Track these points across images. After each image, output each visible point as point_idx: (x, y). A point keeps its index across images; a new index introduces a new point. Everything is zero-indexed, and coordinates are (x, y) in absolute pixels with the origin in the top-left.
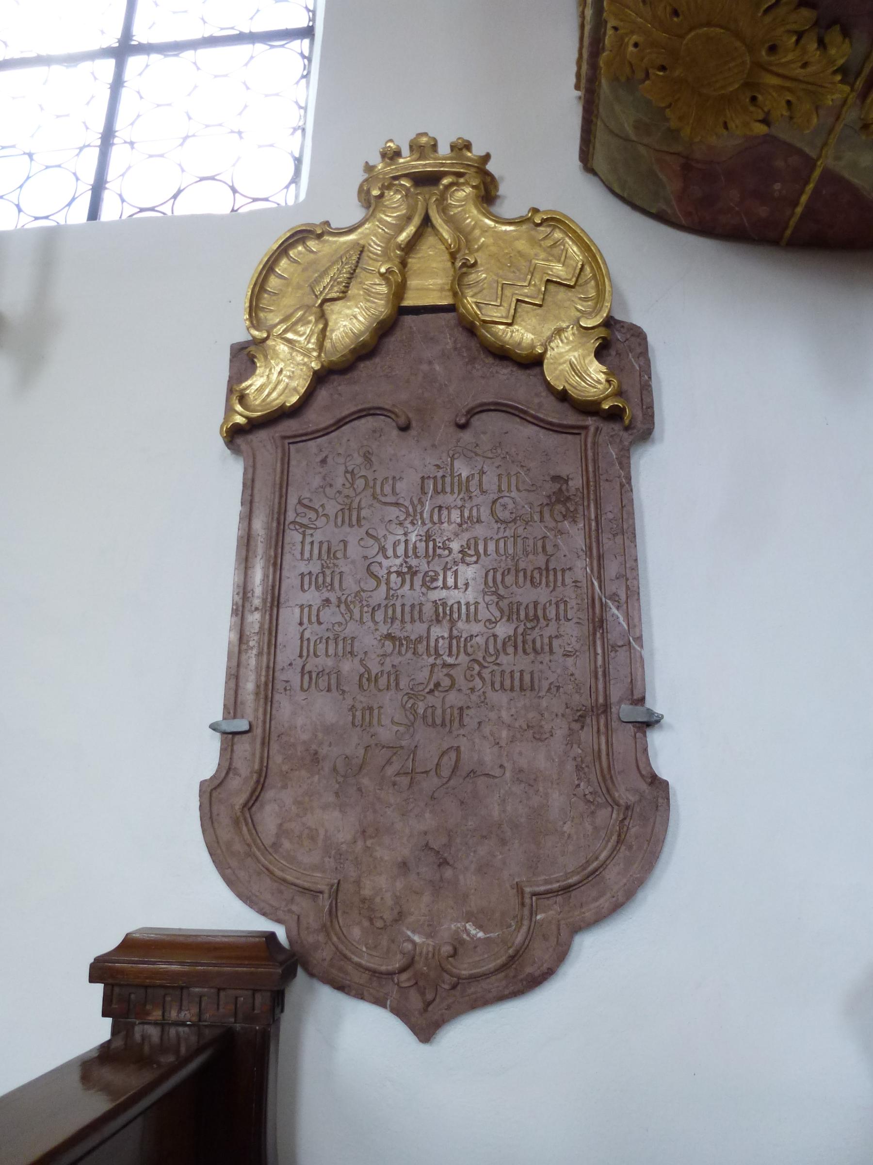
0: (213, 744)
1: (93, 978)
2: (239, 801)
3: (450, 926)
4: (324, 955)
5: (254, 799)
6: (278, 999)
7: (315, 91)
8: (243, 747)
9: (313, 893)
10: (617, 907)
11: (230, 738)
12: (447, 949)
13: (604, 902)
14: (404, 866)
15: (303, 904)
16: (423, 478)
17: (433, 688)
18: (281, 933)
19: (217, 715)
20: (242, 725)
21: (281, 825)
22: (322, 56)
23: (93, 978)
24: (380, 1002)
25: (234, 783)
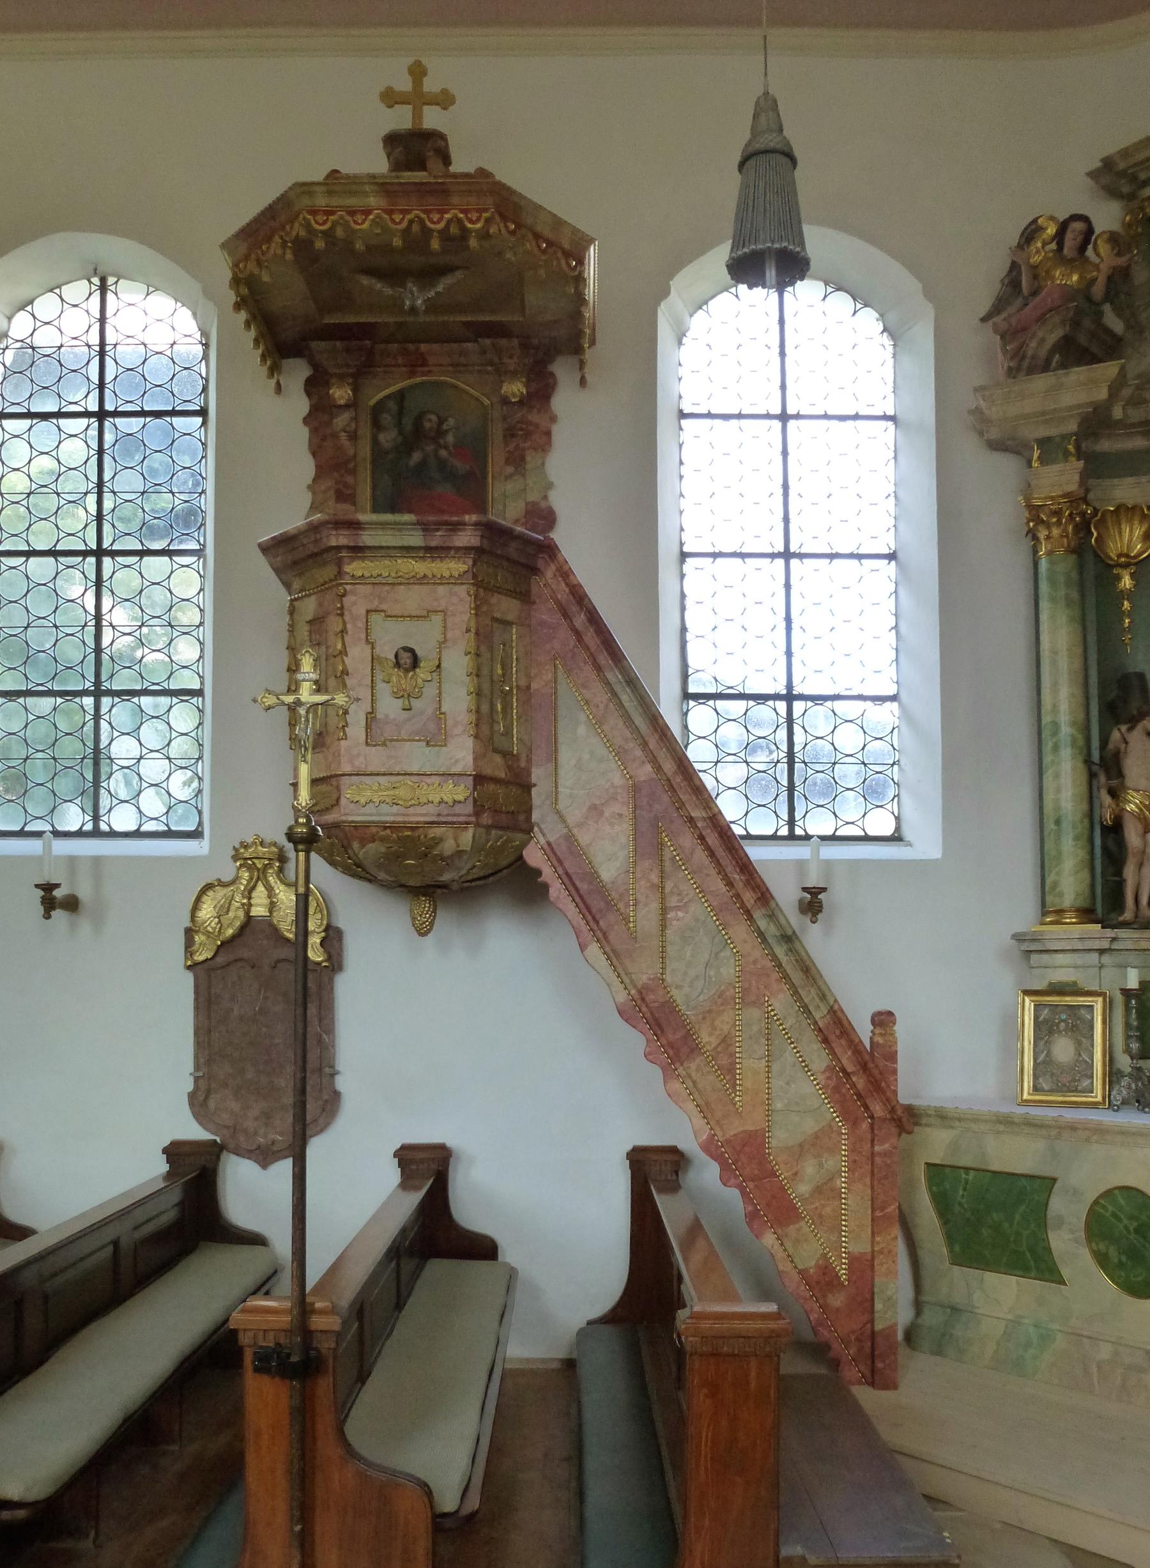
0: (192, 1079)
1: (163, 1153)
2: (202, 1098)
3: (272, 1136)
4: (232, 1146)
5: (207, 1097)
6: (218, 1158)
7: (213, 529)
8: (201, 1082)
9: (228, 1127)
10: (321, 1131)
11: (197, 1079)
12: (270, 1143)
13: (318, 1129)
14: (256, 1119)
15: (225, 1131)
16: (368, 612)
17: (552, 535)
18: (218, 1140)
19: (192, 1070)
20: (201, 1074)
21: (336, 677)
22: (218, 356)
23: (163, 1153)
24: (249, 1158)
25: (199, 1093)
